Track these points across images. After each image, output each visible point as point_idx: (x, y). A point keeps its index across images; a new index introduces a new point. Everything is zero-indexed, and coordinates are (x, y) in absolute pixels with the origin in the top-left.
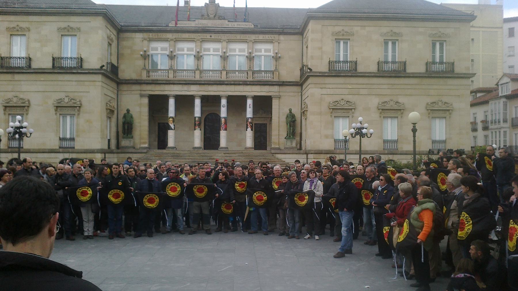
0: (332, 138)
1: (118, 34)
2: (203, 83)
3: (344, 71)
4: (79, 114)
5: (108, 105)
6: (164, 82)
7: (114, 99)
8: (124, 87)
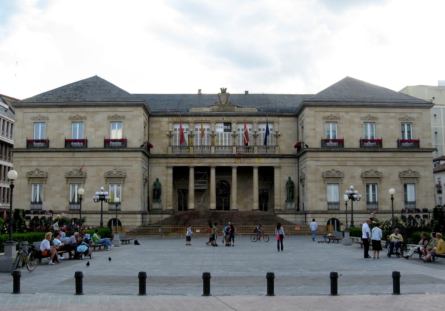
0: (326, 201)
2: (217, 156)
4: (124, 183)
5: (145, 176)
7: (147, 170)
8: (154, 161)
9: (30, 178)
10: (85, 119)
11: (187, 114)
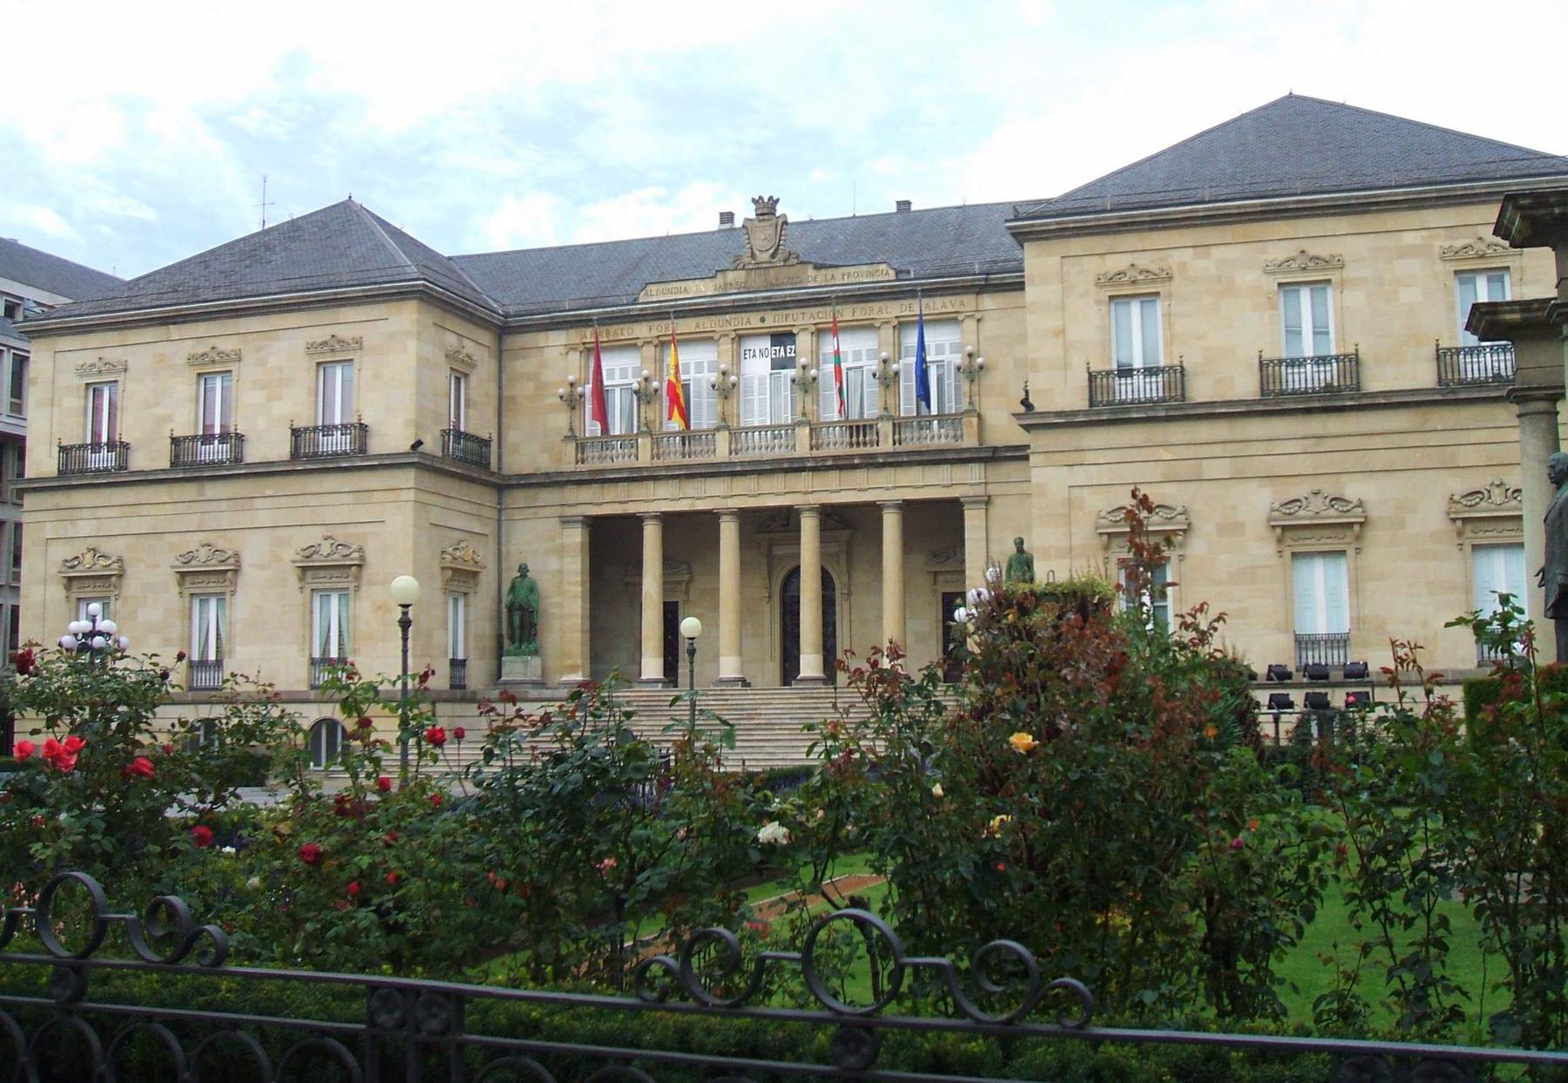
1: (500, 340)
3: (1140, 402)
6: (625, 475)
8: (518, 498)
9: (70, 579)
10: (233, 361)
11: (629, 310)
